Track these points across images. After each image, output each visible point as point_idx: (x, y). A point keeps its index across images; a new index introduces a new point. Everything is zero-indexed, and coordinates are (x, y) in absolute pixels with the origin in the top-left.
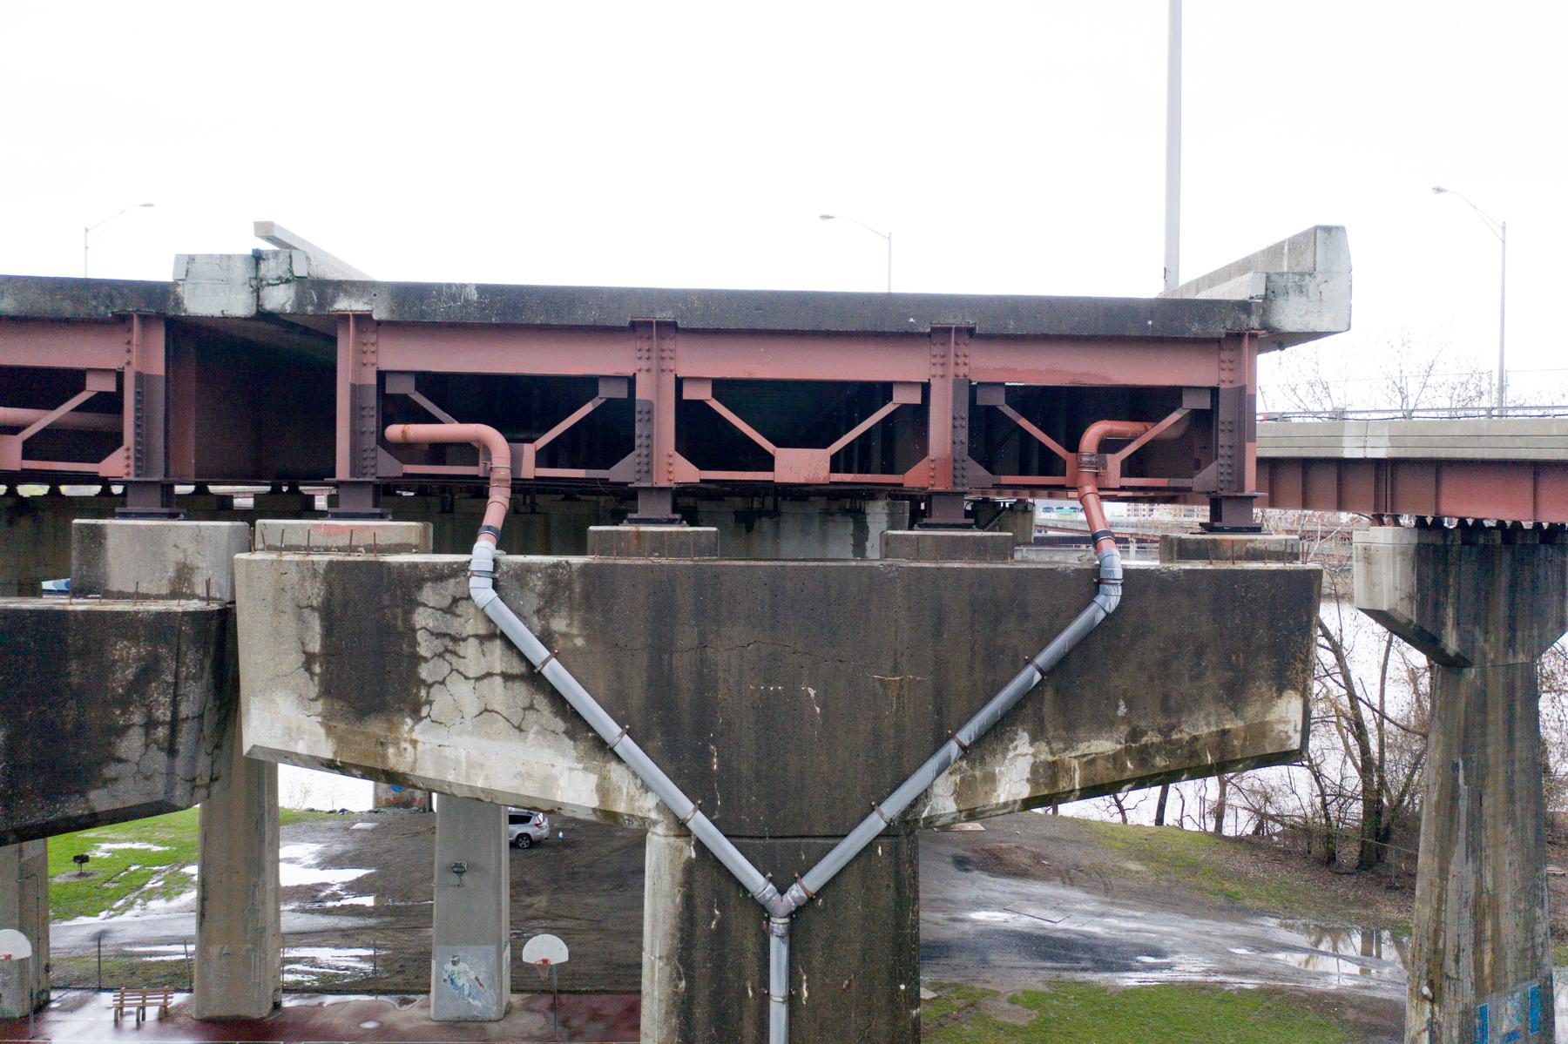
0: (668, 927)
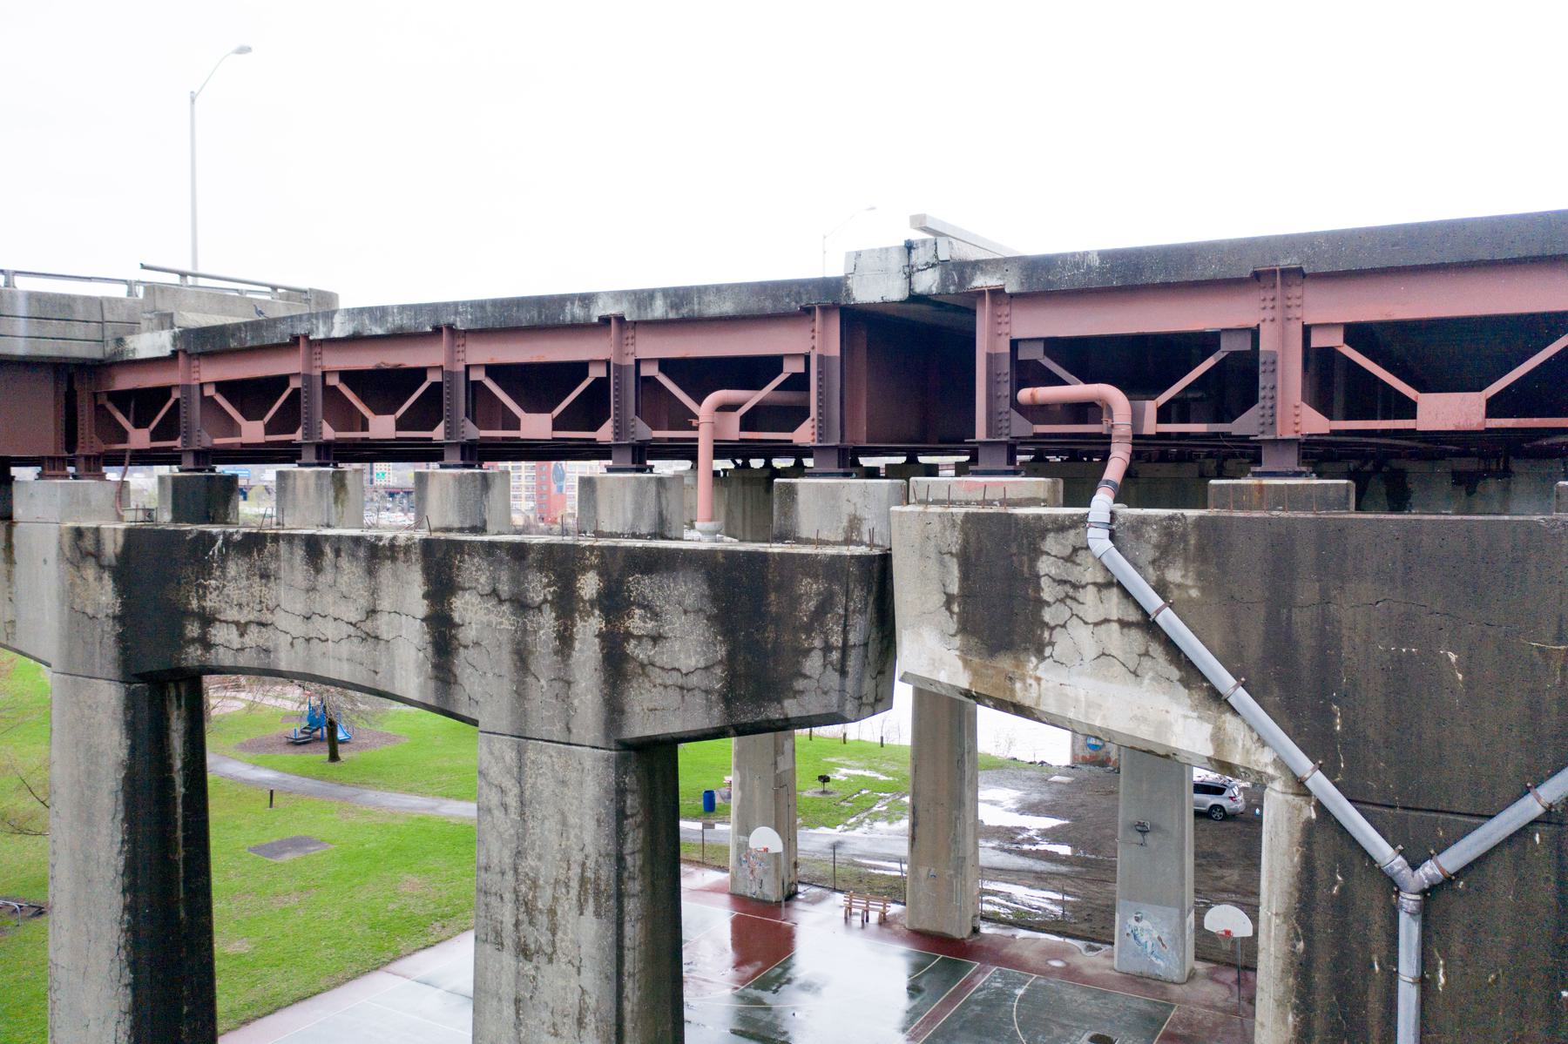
0: (1285, 885)
